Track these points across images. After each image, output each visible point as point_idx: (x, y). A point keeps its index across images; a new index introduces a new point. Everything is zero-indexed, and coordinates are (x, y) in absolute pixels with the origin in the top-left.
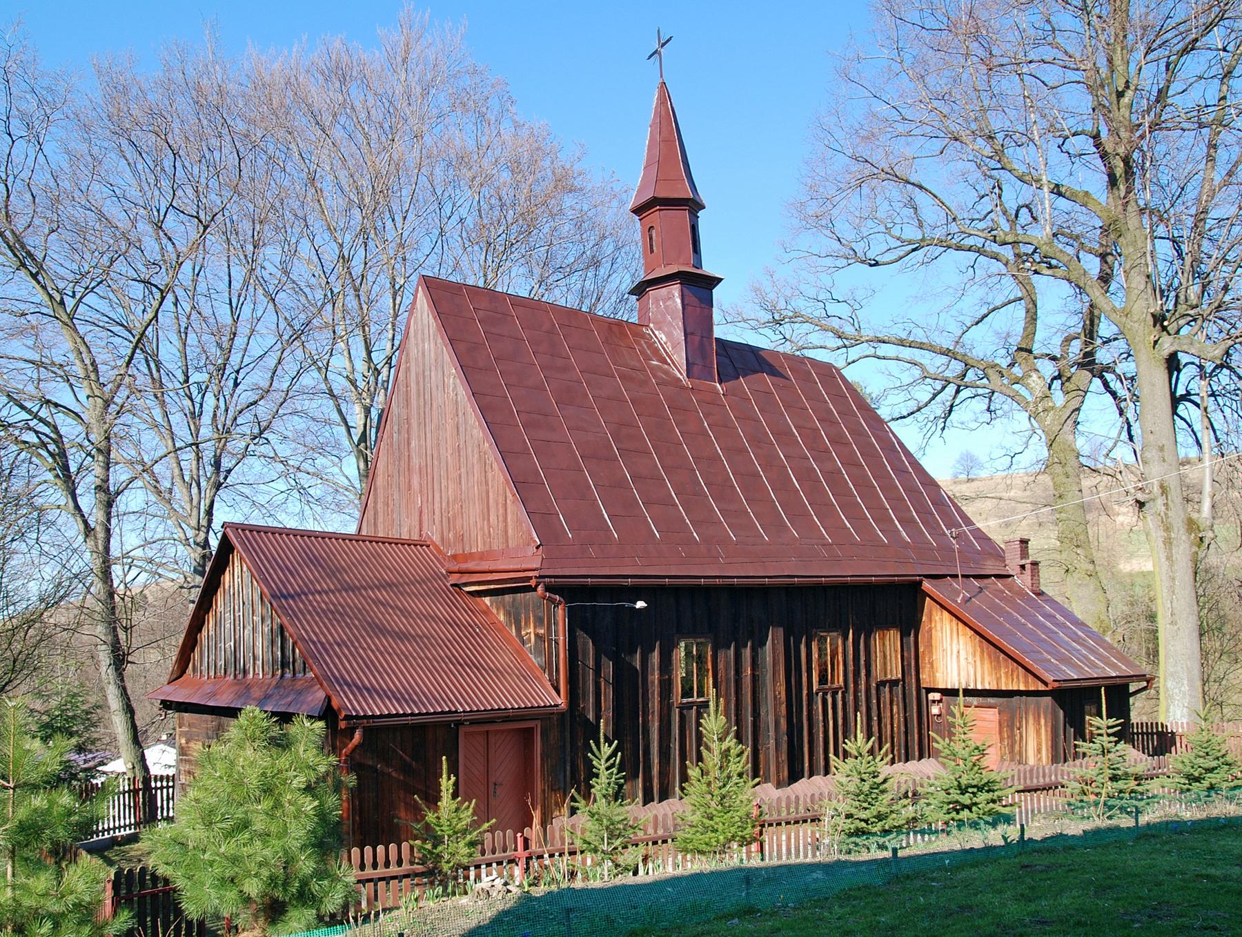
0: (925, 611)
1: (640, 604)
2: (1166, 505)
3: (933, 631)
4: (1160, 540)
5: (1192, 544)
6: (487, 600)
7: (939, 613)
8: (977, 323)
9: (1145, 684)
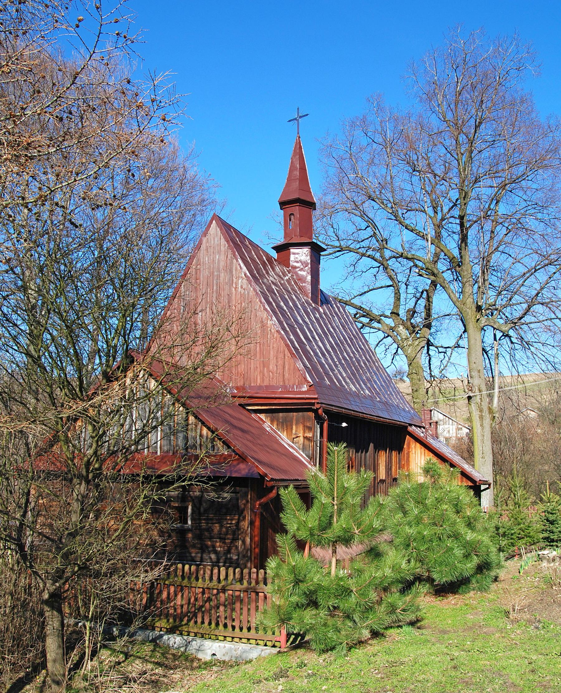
0: (406, 442)
1: (344, 425)
2: (481, 399)
3: (410, 454)
4: (478, 416)
5: (491, 419)
6: (262, 416)
7: (414, 444)
8: (361, 295)
9: (487, 486)
